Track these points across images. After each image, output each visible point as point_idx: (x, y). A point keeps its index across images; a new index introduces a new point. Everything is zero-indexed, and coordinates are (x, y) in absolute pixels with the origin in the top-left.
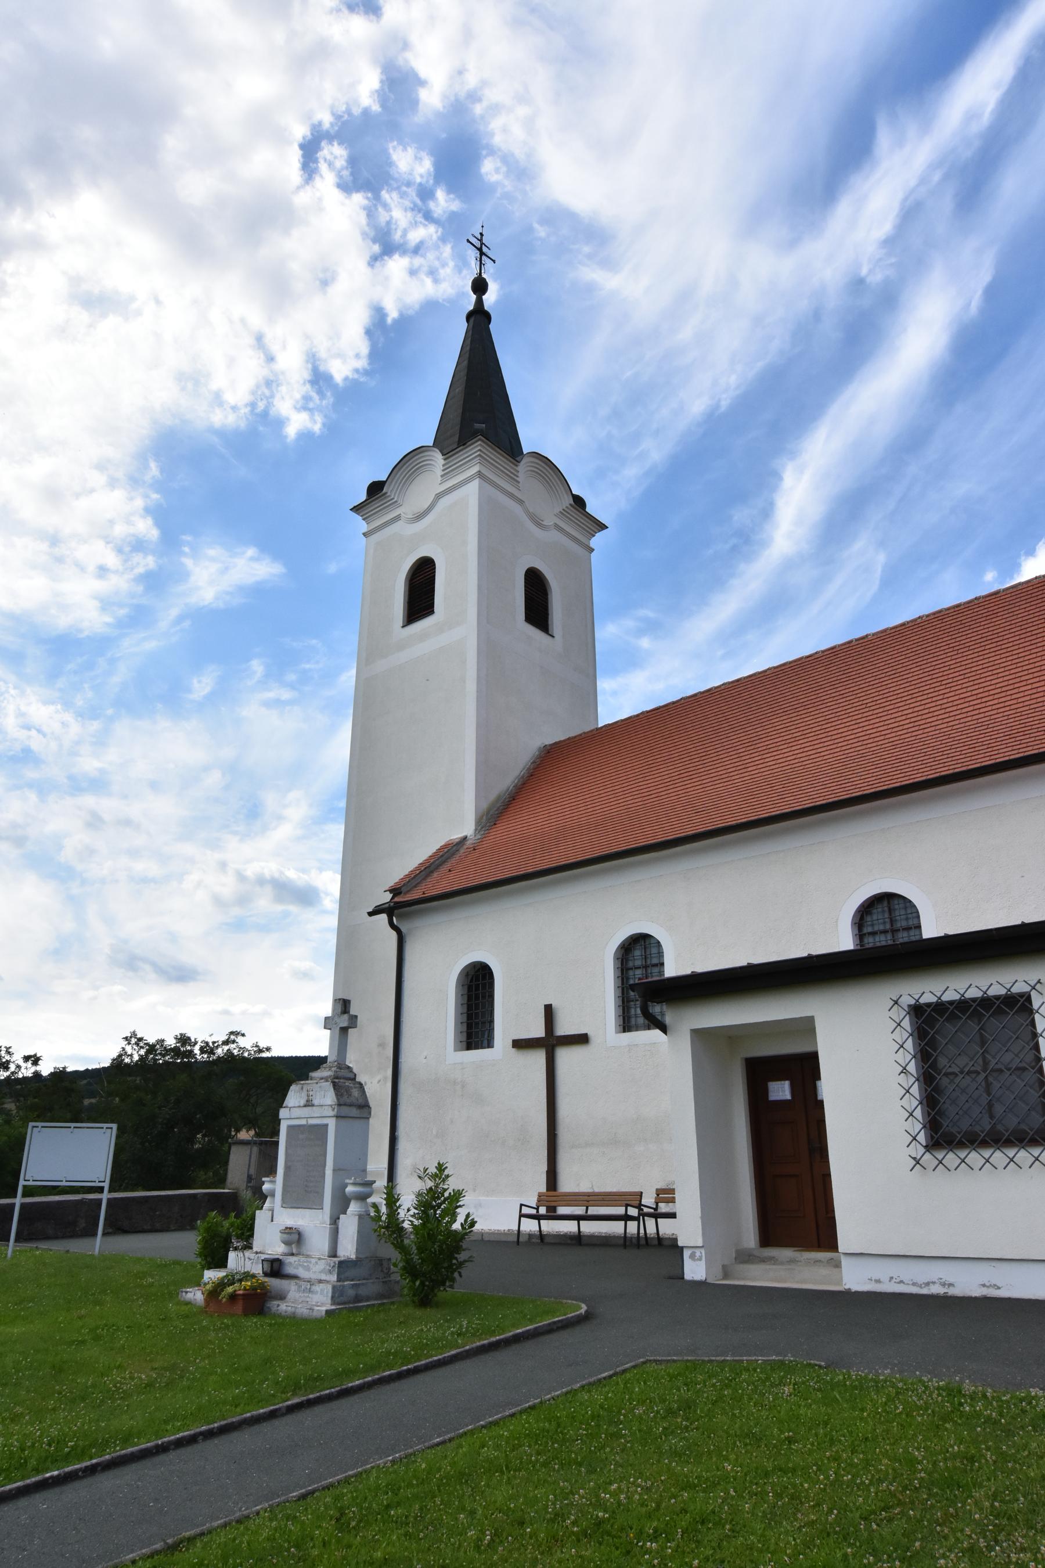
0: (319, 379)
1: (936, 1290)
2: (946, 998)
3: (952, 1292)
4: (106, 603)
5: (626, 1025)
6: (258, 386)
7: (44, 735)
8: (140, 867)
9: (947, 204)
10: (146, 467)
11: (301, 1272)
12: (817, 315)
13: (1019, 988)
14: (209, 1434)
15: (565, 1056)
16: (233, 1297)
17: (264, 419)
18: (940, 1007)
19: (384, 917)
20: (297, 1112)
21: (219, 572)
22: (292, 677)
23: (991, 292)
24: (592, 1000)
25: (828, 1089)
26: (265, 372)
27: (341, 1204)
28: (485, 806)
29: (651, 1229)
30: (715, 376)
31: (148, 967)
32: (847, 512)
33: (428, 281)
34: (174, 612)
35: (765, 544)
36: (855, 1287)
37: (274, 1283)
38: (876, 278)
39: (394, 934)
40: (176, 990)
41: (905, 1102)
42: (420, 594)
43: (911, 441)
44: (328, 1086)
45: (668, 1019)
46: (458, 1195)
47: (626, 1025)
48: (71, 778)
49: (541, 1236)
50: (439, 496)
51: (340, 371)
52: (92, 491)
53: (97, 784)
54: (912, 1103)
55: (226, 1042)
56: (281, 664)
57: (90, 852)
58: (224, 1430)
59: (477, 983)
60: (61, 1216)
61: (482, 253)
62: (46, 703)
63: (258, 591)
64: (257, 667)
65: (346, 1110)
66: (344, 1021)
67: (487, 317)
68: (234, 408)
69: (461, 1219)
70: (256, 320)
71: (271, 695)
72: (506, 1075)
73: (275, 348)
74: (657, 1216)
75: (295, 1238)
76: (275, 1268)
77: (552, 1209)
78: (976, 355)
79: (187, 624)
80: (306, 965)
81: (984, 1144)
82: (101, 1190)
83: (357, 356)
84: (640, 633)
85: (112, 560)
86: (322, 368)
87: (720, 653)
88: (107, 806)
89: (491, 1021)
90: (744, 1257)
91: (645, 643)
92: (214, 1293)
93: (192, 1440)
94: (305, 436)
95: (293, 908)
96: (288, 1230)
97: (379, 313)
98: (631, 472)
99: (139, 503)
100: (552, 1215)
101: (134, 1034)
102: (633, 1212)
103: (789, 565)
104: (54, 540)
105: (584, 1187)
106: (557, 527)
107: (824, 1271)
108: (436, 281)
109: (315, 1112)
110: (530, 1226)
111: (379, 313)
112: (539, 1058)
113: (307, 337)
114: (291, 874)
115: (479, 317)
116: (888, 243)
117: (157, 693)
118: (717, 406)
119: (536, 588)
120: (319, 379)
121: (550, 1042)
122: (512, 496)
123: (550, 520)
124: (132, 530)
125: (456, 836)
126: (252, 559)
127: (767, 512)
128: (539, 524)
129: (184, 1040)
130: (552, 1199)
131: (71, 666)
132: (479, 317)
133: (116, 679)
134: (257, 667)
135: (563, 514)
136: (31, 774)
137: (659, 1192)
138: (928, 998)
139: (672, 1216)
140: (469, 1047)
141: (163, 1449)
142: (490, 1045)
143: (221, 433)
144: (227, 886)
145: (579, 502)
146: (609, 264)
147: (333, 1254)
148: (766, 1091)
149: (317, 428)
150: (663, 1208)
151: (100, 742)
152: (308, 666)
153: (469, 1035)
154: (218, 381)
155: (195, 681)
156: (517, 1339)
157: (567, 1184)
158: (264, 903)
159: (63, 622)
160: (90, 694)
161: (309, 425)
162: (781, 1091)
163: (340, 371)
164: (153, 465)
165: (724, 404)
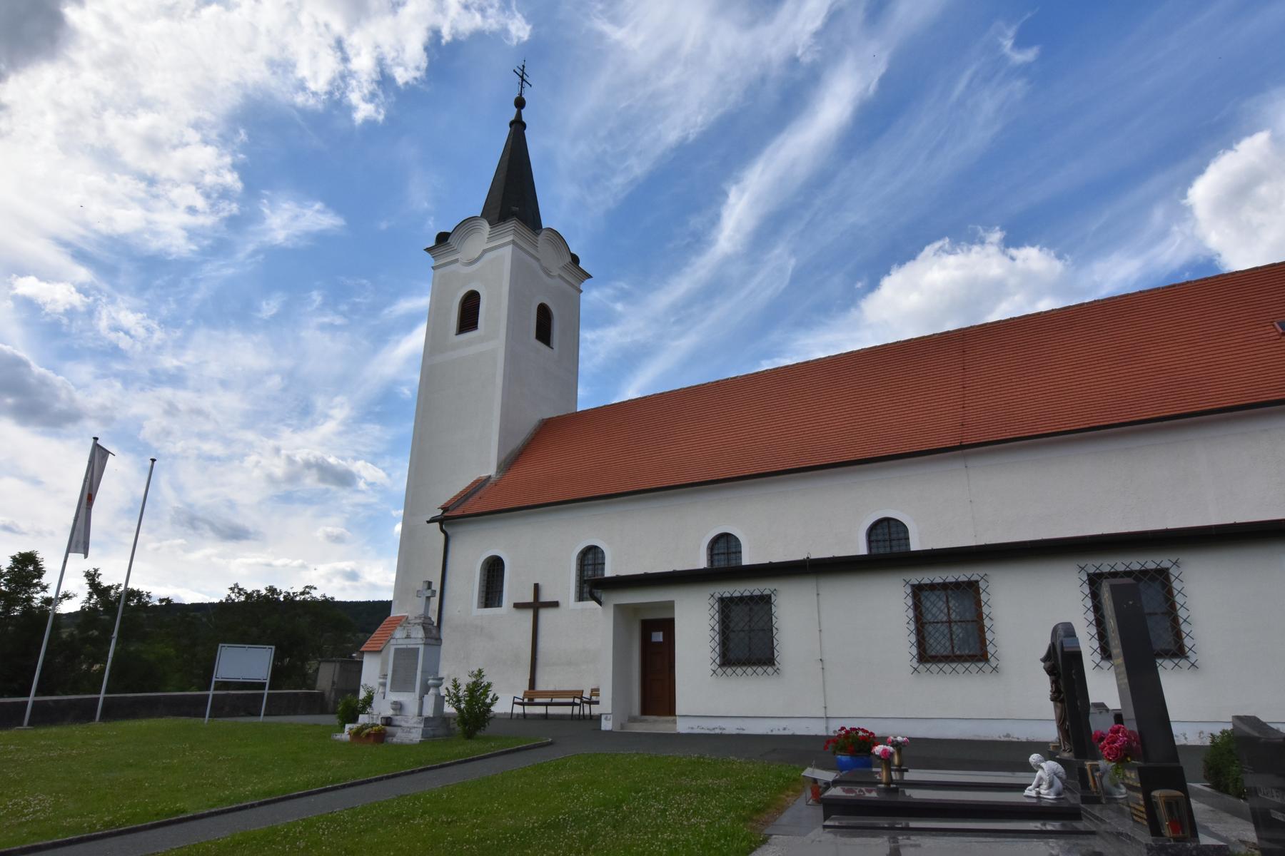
0: (384, 80)
1: (717, 731)
4: (192, 234)
5: (581, 598)
6: (334, 79)
7: (132, 337)
8: (207, 447)
9: (860, 15)
10: (236, 132)
11: (403, 724)
12: (763, 80)
14: (388, 778)
15: (545, 614)
16: (368, 735)
17: (336, 103)
18: (731, 599)
19: (437, 525)
20: (400, 642)
21: (288, 220)
22: (344, 307)
23: (885, 81)
24: (563, 584)
26: (341, 67)
27: (425, 689)
28: (503, 456)
29: (587, 711)
30: (686, 115)
31: (207, 527)
33: (478, 17)
34: (251, 247)
35: (711, 243)
37: (388, 728)
38: (807, 59)
39: (442, 535)
40: (230, 546)
43: (820, 180)
44: (420, 628)
45: (603, 599)
46: (489, 685)
47: (581, 598)
48: (153, 372)
49: (525, 715)
50: (485, 251)
51: (401, 76)
52: (187, 144)
53: (176, 379)
54: (714, 644)
55: (303, 593)
56: (337, 294)
57: (167, 433)
58: (393, 776)
59: (494, 569)
60: (241, 700)
61: (523, 80)
62: (135, 310)
63: (321, 238)
64: (317, 297)
65: (429, 641)
66: (429, 593)
67: (524, 126)
68: (315, 94)
69: (491, 696)
70: (338, 26)
71: (326, 320)
72: (508, 623)
73: (351, 53)
74: (590, 703)
75: (398, 707)
76: (388, 721)
77: (531, 699)
78: (873, 122)
79: (261, 257)
80: (337, 531)
81: (754, 664)
82: (262, 686)
83: (418, 68)
84: (617, 299)
85: (200, 203)
86: (387, 71)
87: (672, 320)
88: (183, 398)
89: (501, 591)
90: (633, 720)
91: (619, 307)
92: (356, 735)
93: (381, 779)
95: (333, 488)
96: (395, 703)
97: (435, 34)
98: (619, 180)
99: (228, 160)
100: (531, 703)
101: (236, 585)
102: (577, 701)
103: (728, 260)
104: (151, 181)
105: (551, 688)
106: (560, 276)
107: (669, 725)
108: (484, 16)
109: (412, 641)
110: (518, 710)
111: (435, 34)
112: (529, 614)
113: (377, 46)
114: (332, 460)
115: (518, 126)
116: (817, 35)
117: (231, 311)
118: (685, 138)
119: (544, 316)
120: (384, 80)
121: (537, 605)
122: (532, 256)
123: (556, 271)
124: (220, 180)
125: (484, 475)
126: (318, 211)
127: (715, 221)
128: (549, 275)
129: (272, 590)
130: (531, 695)
131: (159, 282)
132: (518, 126)
133: (197, 296)
135: (564, 268)
136: (118, 366)
138: (727, 595)
139: (597, 703)
140: (486, 606)
141: (370, 781)
142: (499, 605)
143: (303, 112)
144: (279, 468)
145: (575, 259)
146: (616, 20)
149: (381, 118)
150: (594, 698)
151: (180, 346)
153: (487, 599)
154: (303, 71)
155: (264, 303)
156: (518, 750)
157: (540, 686)
158: (310, 481)
159: (155, 245)
160: (173, 306)
161: (375, 115)
162: (658, 637)
163: (401, 76)
164: (242, 132)
165: (691, 137)
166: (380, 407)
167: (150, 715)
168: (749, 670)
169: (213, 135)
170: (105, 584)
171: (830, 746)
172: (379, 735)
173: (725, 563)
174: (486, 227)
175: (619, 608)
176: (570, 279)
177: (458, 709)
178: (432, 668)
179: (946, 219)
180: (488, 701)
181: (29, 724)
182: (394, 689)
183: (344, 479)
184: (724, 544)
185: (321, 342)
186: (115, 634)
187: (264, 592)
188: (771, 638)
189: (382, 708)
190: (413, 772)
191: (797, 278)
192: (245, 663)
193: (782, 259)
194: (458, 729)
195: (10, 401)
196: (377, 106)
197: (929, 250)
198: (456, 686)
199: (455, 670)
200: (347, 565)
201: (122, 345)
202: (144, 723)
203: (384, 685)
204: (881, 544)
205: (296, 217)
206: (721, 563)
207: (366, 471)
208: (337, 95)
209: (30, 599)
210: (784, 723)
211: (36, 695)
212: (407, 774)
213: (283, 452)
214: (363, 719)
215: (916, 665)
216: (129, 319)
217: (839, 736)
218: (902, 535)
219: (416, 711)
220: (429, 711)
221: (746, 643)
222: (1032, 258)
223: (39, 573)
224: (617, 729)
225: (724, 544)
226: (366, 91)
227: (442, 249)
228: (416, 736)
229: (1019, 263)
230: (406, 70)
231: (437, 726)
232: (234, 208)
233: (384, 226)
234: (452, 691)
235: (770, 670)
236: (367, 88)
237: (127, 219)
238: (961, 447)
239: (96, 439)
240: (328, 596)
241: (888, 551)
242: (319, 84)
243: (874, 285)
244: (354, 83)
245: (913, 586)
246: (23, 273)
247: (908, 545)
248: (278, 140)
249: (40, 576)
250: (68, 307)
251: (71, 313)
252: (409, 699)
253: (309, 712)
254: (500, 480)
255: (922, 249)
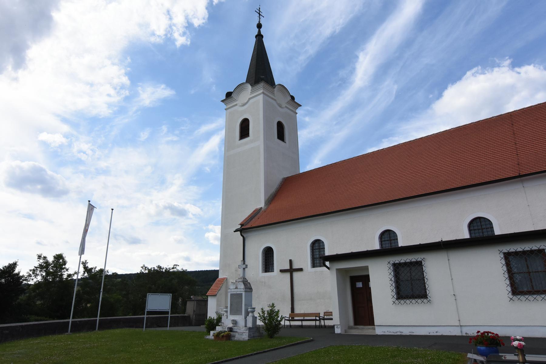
2: (401, 262)
3: (402, 334)
4: (110, 105)
5: (314, 265)
6: (167, 29)
7: (86, 154)
13: (419, 260)
14: (241, 357)
15: (296, 275)
16: (223, 336)
17: (169, 39)
18: (400, 264)
19: (239, 232)
20: (233, 290)
21: (151, 94)
22: (177, 132)
24: (304, 259)
25: (372, 284)
26: (170, 22)
27: (247, 314)
28: (267, 198)
29: (323, 323)
32: (383, 70)
34: (134, 109)
36: (379, 334)
37: (231, 333)
39: (242, 237)
41: (391, 288)
42: (244, 129)
43: (407, 43)
44: (242, 284)
47: (314, 265)
49: (290, 326)
50: (250, 99)
51: (197, 23)
55: (173, 268)
59: (268, 253)
60: (158, 320)
61: (260, 15)
63: (165, 101)
64: (165, 128)
67: (262, 36)
69: (280, 317)
71: (170, 139)
72: (277, 280)
74: (324, 319)
75: (235, 322)
76: (231, 329)
81: (410, 298)
82: (167, 313)
83: (204, 19)
85: (112, 92)
86: (190, 21)
87: (335, 123)
90: (350, 328)
91: (307, 119)
92: (217, 336)
93: (238, 358)
94: (183, 47)
95: (177, 218)
96: (233, 320)
99: (123, 71)
100: (293, 320)
102: (318, 318)
104: (92, 85)
105: (302, 312)
107: (371, 331)
109: (239, 290)
112: (288, 275)
114: (176, 204)
115: (259, 37)
117: (127, 138)
118: (335, 32)
119: (280, 127)
120: (189, 26)
121: (291, 270)
122: (272, 99)
125: (259, 207)
127: (353, 71)
128: (281, 107)
129: (159, 267)
132: (259, 37)
134: (165, 128)
135: (288, 103)
136: (82, 168)
137: (325, 313)
138: (397, 262)
142: (273, 271)
143: (155, 45)
144: (152, 210)
145: (293, 98)
147: (246, 326)
148: (355, 285)
149: (189, 43)
152: (183, 128)
156: (298, 344)
157: (297, 311)
158: (167, 214)
160: (103, 139)
162: (359, 285)
163: (197, 23)
164: (128, 58)
165: (337, 31)
166: (199, 177)
167: (118, 327)
168: (414, 301)
169: (116, 61)
170: (90, 267)
171: (473, 340)
172: (228, 336)
173: (389, 246)
174: (249, 87)
175: (338, 270)
176: (291, 108)
177: (265, 323)
178: (249, 303)
179: (479, 55)
180: (279, 319)
181: (71, 332)
182: (231, 314)
183: (182, 213)
184: (388, 236)
185: (168, 149)
186: (102, 290)
187: (156, 268)
188: (424, 283)
189: (227, 322)
190: (252, 355)
191: (398, 96)
192: (159, 302)
193: (390, 86)
194: (265, 333)
195: (39, 187)
196: (187, 38)
197: (469, 73)
198: (263, 312)
199: (261, 303)
200: (185, 254)
201: (83, 159)
202: (118, 331)
203: (227, 312)
204: (477, 231)
205: (153, 93)
206: (387, 246)
207: (192, 209)
208: (169, 35)
209: (62, 275)
210: (436, 329)
211: (73, 318)
212: (249, 356)
213: (154, 202)
214: (218, 329)
215: (511, 297)
216: (85, 147)
217: (478, 336)
218: (489, 226)
219: (244, 324)
220: (250, 324)
221: (411, 286)
222: (530, 71)
223: (65, 263)
224: (343, 333)
225: (388, 236)
226: (181, 32)
227: (229, 100)
228: (245, 337)
229: (522, 74)
230: (198, 19)
231: (254, 330)
232: (127, 93)
233: (192, 92)
234: (261, 314)
235: (425, 301)
236: (181, 30)
237: (82, 103)
238: (520, 176)
239: (89, 201)
240: (184, 269)
241: (481, 236)
242: (161, 32)
243: (440, 96)
244: (174, 28)
245: (504, 253)
246: (41, 131)
247: (493, 231)
248: (148, 61)
249: (65, 265)
250: (60, 143)
251: (61, 146)
252: (240, 319)
253: (184, 325)
254: (267, 209)
255: (465, 74)
